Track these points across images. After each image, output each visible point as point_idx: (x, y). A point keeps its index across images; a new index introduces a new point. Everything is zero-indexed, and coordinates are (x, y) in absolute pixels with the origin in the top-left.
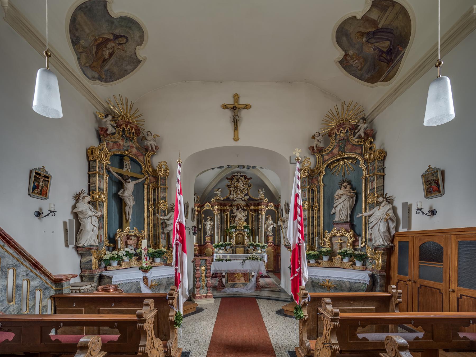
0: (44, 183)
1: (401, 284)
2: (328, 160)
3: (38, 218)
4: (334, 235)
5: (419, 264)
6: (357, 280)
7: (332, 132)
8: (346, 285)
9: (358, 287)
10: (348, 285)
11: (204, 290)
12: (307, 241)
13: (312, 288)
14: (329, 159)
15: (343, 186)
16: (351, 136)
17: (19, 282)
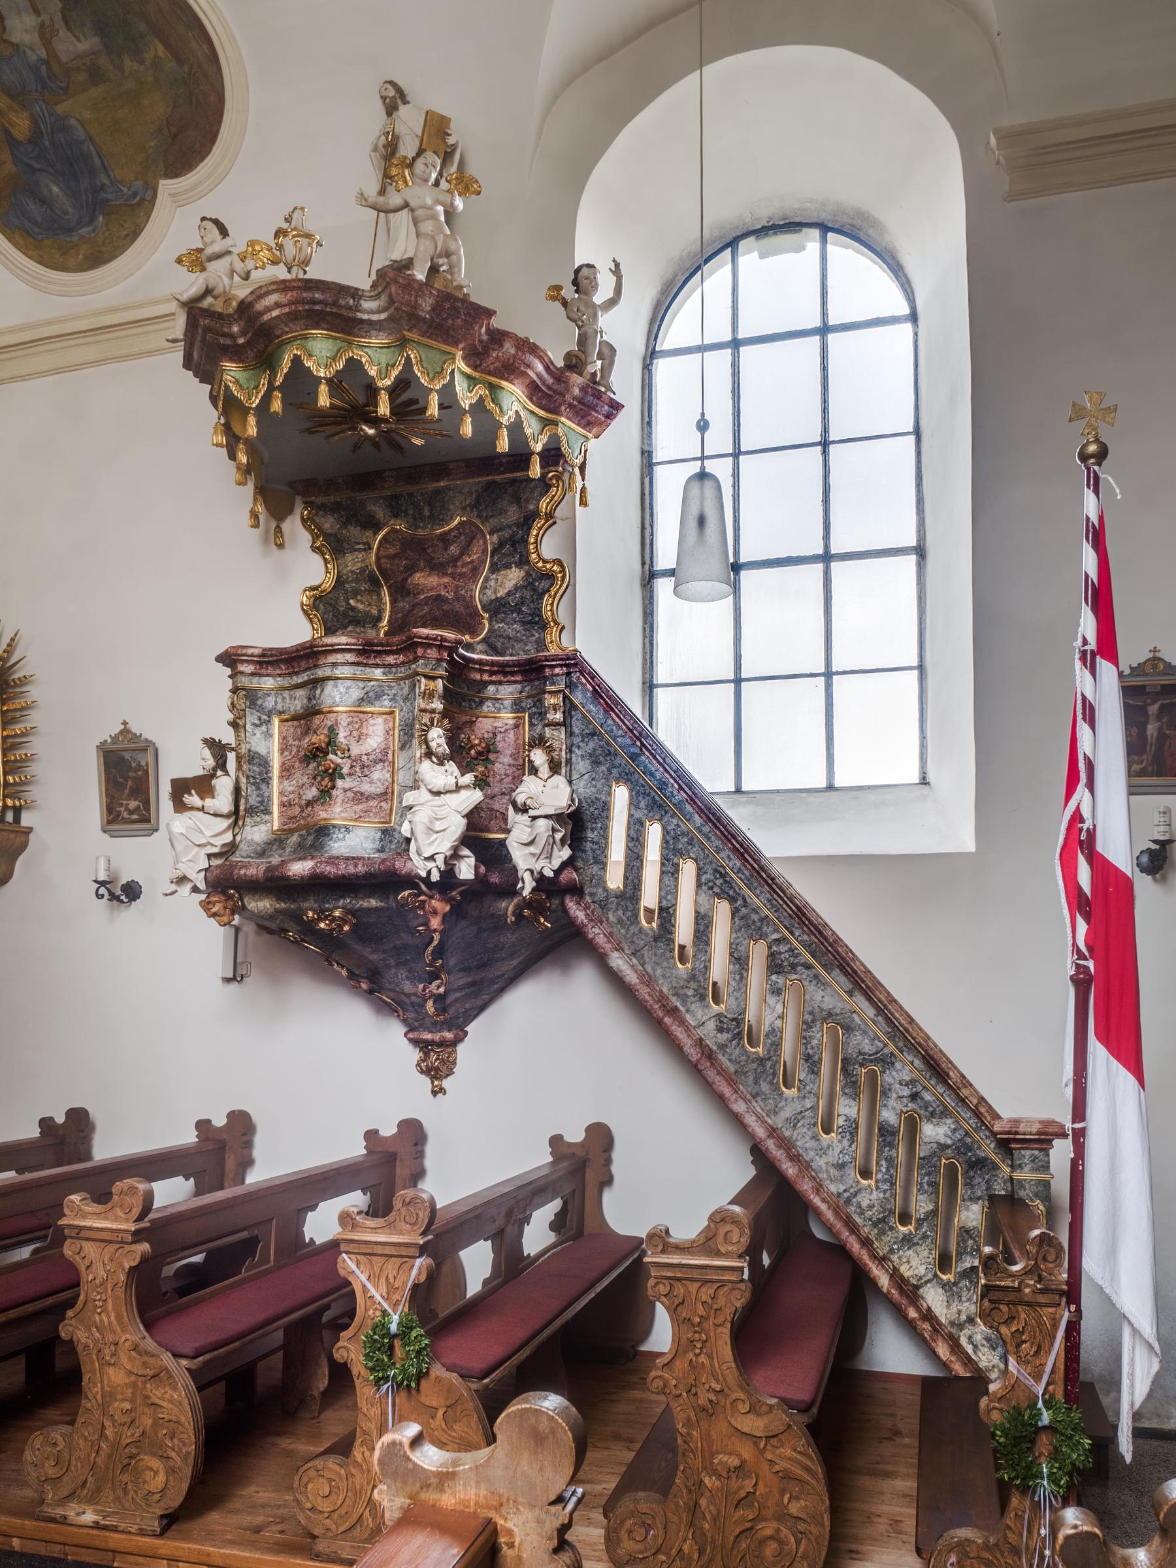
0: (1165, 720)
3: (1155, 879)
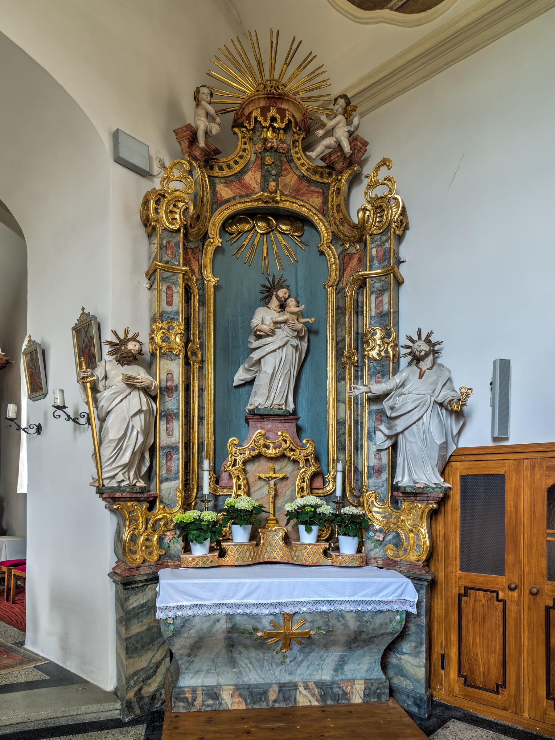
1: (476, 600)
2: (228, 201)
4: (259, 452)
5: (548, 539)
6: (381, 602)
7: (246, 112)
8: (346, 626)
9: (381, 625)
10: (353, 624)
12: (178, 472)
13: (224, 651)
14: (234, 198)
15: (277, 297)
16: (296, 147)
17: (341, 415)
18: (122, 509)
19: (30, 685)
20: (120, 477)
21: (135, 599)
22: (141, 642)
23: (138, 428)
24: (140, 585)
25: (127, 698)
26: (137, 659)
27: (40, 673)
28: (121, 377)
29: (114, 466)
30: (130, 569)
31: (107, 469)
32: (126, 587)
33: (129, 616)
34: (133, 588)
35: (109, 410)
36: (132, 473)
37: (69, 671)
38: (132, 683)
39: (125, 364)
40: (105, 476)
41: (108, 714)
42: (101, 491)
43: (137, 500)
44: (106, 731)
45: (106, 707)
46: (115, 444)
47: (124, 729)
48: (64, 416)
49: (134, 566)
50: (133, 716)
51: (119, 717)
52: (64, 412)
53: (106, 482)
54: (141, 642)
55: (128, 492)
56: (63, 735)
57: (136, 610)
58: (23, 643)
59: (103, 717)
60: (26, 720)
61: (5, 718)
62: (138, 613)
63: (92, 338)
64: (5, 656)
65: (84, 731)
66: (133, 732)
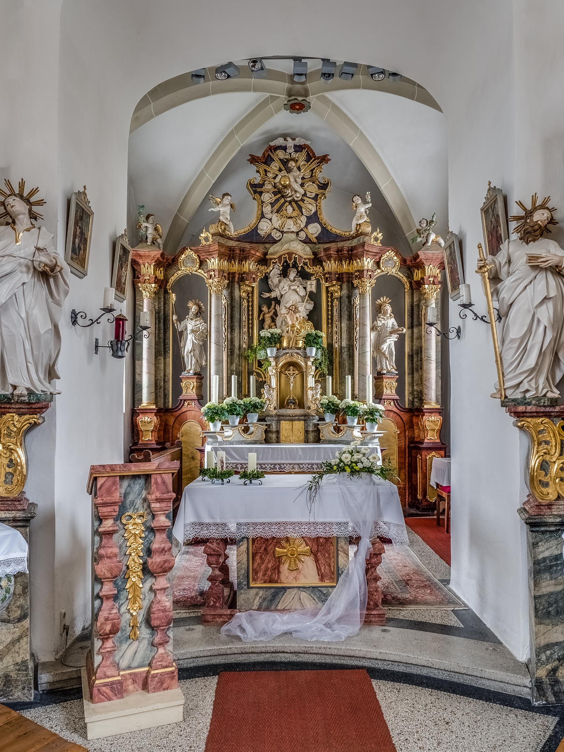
11: (136, 644)
18: (528, 427)
19: (445, 629)
20: (525, 386)
21: (546, 546)
22: (555, 605)
23: (545, 321)
24: (553, 528)
25: (537, 675)
26: (550, 627)
27: (456, 618)
28: (525, 259)
29: (518, 371)
30: (539, 506)
31: (510, 376)
32: (534, 529)
33: (538, 567)
34: (544, 532)
35: (510, 303)
36: (542, 380)
37: (485, 625)
38: (543, 657)
39: (530, 241)
40: (508, 385)
41: (517, 689)
42: (505, 403)
43: (547, 415)
44: (509, 708)
45: (513, 679)
46: (516, 345)
47: (531, 714)
48: (470, 315)
49: (544, 502)
50: (544, 702)
51: (529, 697)
52: (470, 309)
53: (509, 393)
54: (555, 605)
55: (534, 405)
56: (464, 695)
57: (548, 561)
58: (447, 582)
59: (510, 690)
60: (430, 665)
61: (411, 656)
62: (551, 567)
63: (498, 216)
64: (429, 591)
65: (486, 699)
66: (539, 721)
